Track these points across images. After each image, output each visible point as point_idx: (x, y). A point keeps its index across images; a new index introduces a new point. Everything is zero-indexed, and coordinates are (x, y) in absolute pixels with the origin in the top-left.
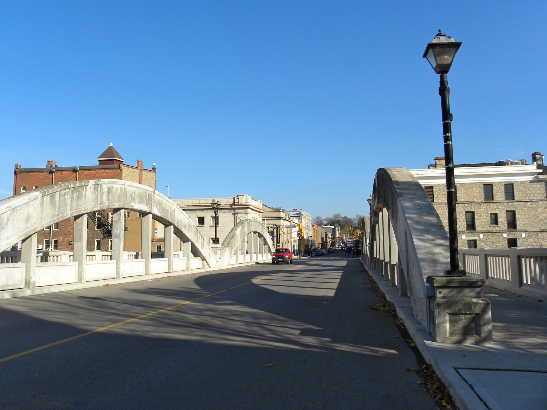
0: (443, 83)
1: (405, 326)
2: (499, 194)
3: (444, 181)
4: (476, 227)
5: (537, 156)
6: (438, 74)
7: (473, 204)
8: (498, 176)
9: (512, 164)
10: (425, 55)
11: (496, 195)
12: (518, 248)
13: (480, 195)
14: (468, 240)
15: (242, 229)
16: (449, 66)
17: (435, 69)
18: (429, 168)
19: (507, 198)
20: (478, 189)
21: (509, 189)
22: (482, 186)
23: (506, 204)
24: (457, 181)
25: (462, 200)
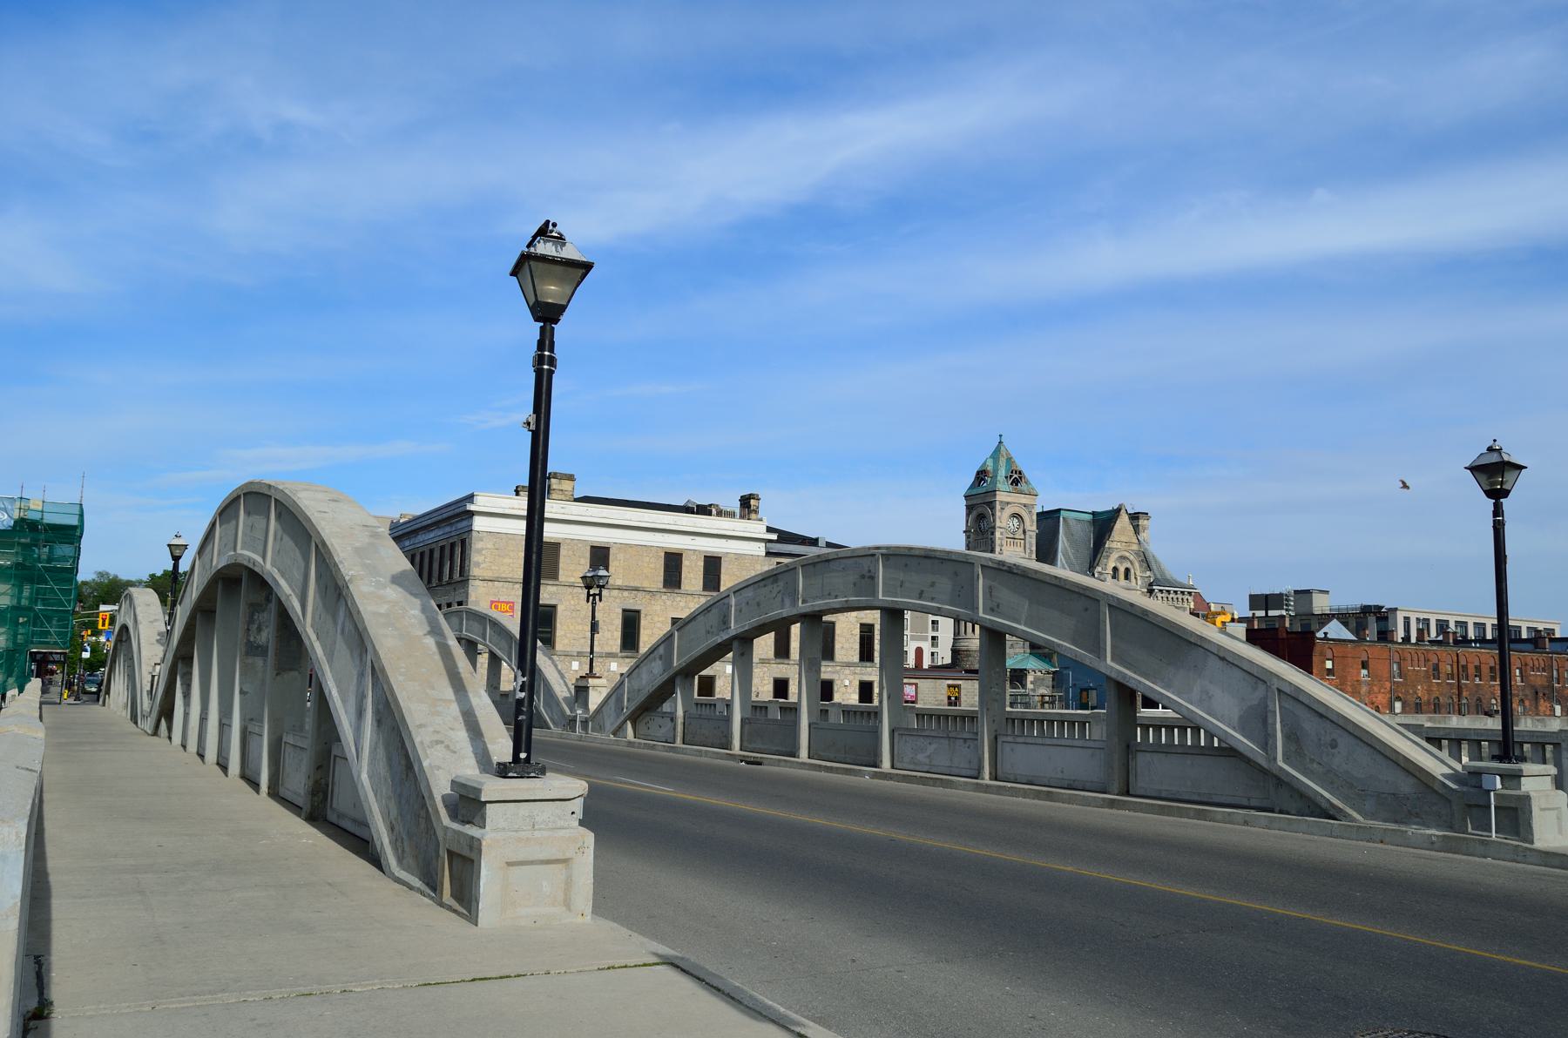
0: (546, 342)
2: (692, 576)
6: (536, 320)
8: (694, 539)
9: (720, 513)
10: (514, 273)
11: (455, 719)
12: (996, 556)
13: (655, 573)
16: (561, 309)
17: (531, 309)
21: (712, 565)
25: (619, 582)
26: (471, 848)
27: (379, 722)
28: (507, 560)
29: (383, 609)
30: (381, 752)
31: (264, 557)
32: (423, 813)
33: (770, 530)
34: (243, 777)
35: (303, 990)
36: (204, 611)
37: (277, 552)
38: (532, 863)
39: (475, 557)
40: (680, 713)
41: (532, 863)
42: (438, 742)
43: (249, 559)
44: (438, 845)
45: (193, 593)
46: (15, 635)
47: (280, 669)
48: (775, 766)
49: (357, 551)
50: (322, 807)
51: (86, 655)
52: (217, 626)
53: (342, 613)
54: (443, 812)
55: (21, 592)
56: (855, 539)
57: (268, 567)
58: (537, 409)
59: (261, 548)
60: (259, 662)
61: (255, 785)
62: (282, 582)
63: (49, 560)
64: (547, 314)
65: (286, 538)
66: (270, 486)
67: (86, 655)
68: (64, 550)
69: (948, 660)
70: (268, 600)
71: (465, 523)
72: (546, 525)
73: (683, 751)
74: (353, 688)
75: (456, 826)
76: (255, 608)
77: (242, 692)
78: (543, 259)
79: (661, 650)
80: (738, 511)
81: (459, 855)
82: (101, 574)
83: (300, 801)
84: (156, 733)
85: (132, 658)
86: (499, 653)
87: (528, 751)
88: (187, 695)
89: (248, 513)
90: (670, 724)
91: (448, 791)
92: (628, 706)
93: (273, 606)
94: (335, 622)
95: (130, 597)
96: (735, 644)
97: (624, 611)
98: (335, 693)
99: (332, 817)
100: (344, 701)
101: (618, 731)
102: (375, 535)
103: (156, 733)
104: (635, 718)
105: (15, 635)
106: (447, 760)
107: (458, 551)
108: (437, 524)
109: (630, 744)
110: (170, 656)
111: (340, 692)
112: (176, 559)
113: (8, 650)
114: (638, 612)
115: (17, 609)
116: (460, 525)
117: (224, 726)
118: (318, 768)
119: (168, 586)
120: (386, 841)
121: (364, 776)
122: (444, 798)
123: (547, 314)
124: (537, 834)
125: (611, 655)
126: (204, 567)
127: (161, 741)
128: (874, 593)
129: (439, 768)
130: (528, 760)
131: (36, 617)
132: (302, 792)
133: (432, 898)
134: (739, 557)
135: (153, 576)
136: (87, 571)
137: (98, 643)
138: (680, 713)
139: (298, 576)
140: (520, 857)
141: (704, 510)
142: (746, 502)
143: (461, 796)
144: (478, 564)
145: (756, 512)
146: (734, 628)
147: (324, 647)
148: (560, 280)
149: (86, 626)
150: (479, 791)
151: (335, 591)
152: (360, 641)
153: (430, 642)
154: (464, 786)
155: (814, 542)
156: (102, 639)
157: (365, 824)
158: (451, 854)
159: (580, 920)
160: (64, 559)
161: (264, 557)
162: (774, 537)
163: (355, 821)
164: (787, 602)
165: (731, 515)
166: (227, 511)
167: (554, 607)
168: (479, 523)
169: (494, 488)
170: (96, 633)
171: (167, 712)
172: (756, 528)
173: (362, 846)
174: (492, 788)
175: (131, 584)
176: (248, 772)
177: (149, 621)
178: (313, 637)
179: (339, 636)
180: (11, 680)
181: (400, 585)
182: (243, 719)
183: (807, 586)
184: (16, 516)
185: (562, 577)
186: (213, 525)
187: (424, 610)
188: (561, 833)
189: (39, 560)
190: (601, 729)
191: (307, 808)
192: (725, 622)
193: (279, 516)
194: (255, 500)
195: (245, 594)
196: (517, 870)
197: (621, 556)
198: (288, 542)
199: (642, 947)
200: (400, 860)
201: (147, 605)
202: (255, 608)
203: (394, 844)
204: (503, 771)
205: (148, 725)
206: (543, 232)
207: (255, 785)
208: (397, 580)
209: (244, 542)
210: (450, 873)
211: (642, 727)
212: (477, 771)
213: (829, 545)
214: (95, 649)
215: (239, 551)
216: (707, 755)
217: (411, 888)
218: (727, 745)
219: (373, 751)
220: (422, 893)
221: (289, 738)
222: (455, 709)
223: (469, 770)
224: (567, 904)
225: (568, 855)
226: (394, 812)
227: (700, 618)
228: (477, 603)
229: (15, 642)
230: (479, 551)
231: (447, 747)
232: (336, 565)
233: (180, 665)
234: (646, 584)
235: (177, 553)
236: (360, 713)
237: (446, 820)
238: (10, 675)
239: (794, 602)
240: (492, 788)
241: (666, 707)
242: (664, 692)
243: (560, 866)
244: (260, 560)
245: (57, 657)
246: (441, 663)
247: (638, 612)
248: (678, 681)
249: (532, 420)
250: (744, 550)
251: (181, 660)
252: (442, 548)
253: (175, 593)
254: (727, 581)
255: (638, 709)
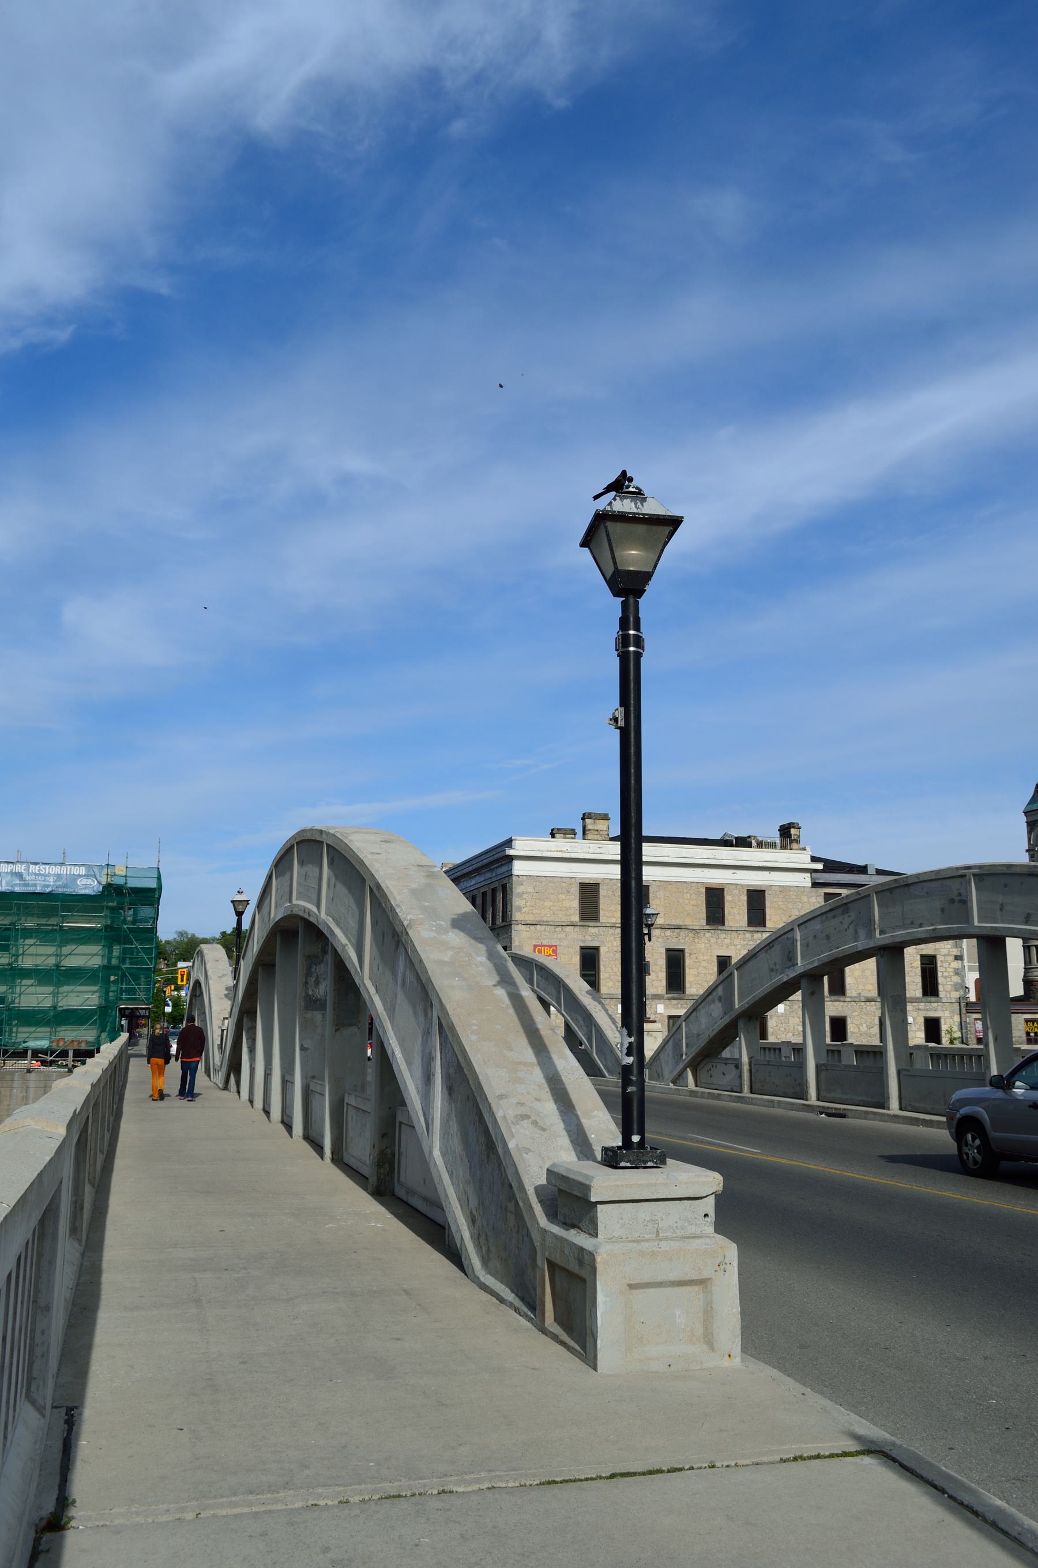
1: (594, 1260)
2: (736, 911)
3: (615, 871)
4: (687, 985)
5: (793, 831)
6: (616, 594)
7: (682, 933)
8: (736, 873)
9: (760, 845)
10: (585, 544)
14: (670, 1017)
15: (154, 1032)
16: (646, 577)
18: (553, 835)
19: (750, 923)
20: (694, 896)
21: (756, 899)
22: (704, 890)
23: (748, 935)
24: (649, 874)
26: (581, 1262)
27: (450, 1089)
28: (548, 904)
29: (447, 956)
30: (454, 1127)
31: (318, 907)
32: (511, 1206)
33: (814, 859)
34: (307, 1137)
35: (391, 1488)
36: (265, 965)
37: (331, 900)
38: (660, 1284)
39: (517, 902)
40: (745, 1059)
41: (660, 1284)
42: (525, 1117)
43: (305, 909)
44: (534, 1250)
45: (254, 947)
46: (107, 993)
47: (339, 1025)
48: (861, 1120)
49: (414, 892)
50: (389, 1179)
51: (168, 1009)
52: (277, 979)
53: (401, 962)
54: (538, 1209)
55: (110, 952)
56: (912, 862)
57: (323, 917)
58: (624, 701)
59: (315, 897)
60: (318, 1015)
61: (319, 1148)
62: (338, 931)
63: (134, 922)
64: (628, 586)
65: (339, 886)
66: (321, 832)
67: (168, 1009)
68: (145, 911)
69: (1021, 992)
70: (325, 952)
71: (505, 869)
72: (619, 858)
73: (752, 1102)
74: (418, 1048)
75: (556, 1229)
76: (312, 960)
77: (303, 1048)
78: (623, 518)
79: (720, 991)
80: (778, 841)
81: (563, 1269)
82: (181, 934)
83: (366, 1171)
84: (226, 1087)
85: (204, 1013)
86: (547, 998)
87: (641, 1132)
88: (252, 1050)
89: (301, 863)
90: (735, 1072)
91: (543, 1181)
92: (687, 1053)
93: (329, 958)
94: (394, 974)
95: (201, 953)
96: (804, 983)
97: (582, 948)
98: (398, 1053)
99: (401, 1193)
100: (409, 1064)
101: (679, 1079)
102: (431, 875)
103: (226, 1087)
104: (696, 1064)
105: (107, 993)
106: (539, 1149)
107: (499, 896)
108: (477, 871)
109: (692, 1093)
110: (236, 1010)
111: (404, 1051)
112: (239, 914)
113: (100, 1007)
114: (682, 951)
115: (108, 968)
116: (500, 871)
117: (286, 1083)
118: (384, 1135)
119: (234, 942)
120: (466, 1235)
121: (437, 1153)
122: (538, 1190)
123: (628, 586)
124: (664, 1245)
125: (657, 997)
126: (262, 920)
127: (232, 1094)
128: (967, 918)
129: (528, 1150)
130: (642, 1143)
131: (124, 975)
132: (367, 1160)
133: (530, 1320)
134: (783, 889)
135: (224, 934)
136: (167, 930)
137: (179, 997)
138: (745, 1059)
139: (353, 924)
140: (646, 1278)
141: (743, 842)
142: (785, 831)
143: (560, 1191)
144: (520, 909)
145: (797, 841)
146: (801, 964)
147: (383, 1000)
148: (644, 543)
149: (168, 982)
150: (587, 1188)
151: (393, 938)
152: (423, 994)
153: (501, 993)
154: (565, 1178)
155: (863, 870)
156: (183, 993)
157: (438, 1205)
158: (552, 1265)
159: (726, 1363)
160: (145, 920)
161: (318, 907)
162: (820, 866)
163: (425, 1199)
164: (862, 933)
165: (772, 845)
166: (282, 863)
167: (597, 949)
168: (519, 868)
169: (530, 832)
170: (178, 988)
171: (235, 1067)
172: (800, 858)
173: (435, 1232)
174: (604, 1183)
175: (206, 941)
176: (313, 1134)
177: (219, 979)
178: (372, 990)
179: (400, 995)
180: (104, 1035)
181: (462, 929)
182: (304, 1077)
183: (872, 914)
184: (104, 881)
185: (603, 918)
186: (269, 878)
187: (492, 956)
188: (695, 1244)
189: (125, 921)
190: (659, 1077)
191: (373, 1180)
192: (790, 959)
193: (331, 863)
194: (308, 848)
195: (303, 946)
196: (641, 1294)
197: (661, 894)
198: (341, 889)
199: (823, 1420)
200: (485, 1262)
201: (216, 958)
202: (312, 960)
203: (476, 1239)
204: (612, 1159)
205: (219, 1079)
206: (620, 485)
207: (319, 1148)
208: (459, 923)
209: (299, 893)
210: (560, 1296)
211: (703, 1075)
212: (576, 1159)
213: (880, 872)
214: (177, 1003)
215: (295, 902)
216: (778, 1106)
217: (502, 1300)
218: (803, 1095)
219: (445, 1123)
220: (517, 1310)
221: (350, 1100)
222: (537, 1075)
223: (564, 1156)
224: (709, 1340)
225: (706, 1274)
226: (474, 1203)
227: (762, 956)
228: (521, 947)
229: (107, 1000)
230: (520, 895)
231: (535, 1123)
232: (392, 909)
233: (245, 1020)
234: (688, 922)
235: (240, 908)
236: (428, 1078)
237: (543, 1221)
238: (103, 1030)
239: (870, 934)
240: (604, 1183)
241: (726, 1054)
242: (726, 1036)
243: (696, 1288)
244: (314, 909)
245: (142, 1012)
246: (515, 1019)
247: (682, 951)
248: (741, 1025)
249: (620, 714)
250: (790, 885)
251: (246, 1015)
252: (484, 894)
253: (239, 949)
254: (776, 919)
255: (698, 1055)
